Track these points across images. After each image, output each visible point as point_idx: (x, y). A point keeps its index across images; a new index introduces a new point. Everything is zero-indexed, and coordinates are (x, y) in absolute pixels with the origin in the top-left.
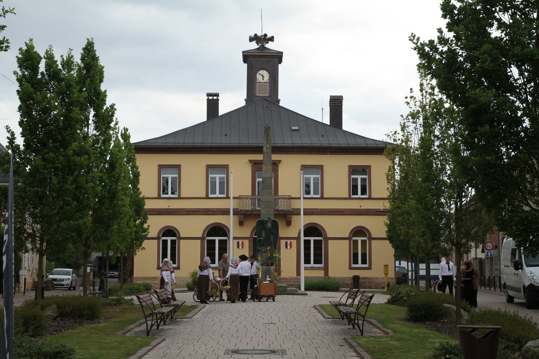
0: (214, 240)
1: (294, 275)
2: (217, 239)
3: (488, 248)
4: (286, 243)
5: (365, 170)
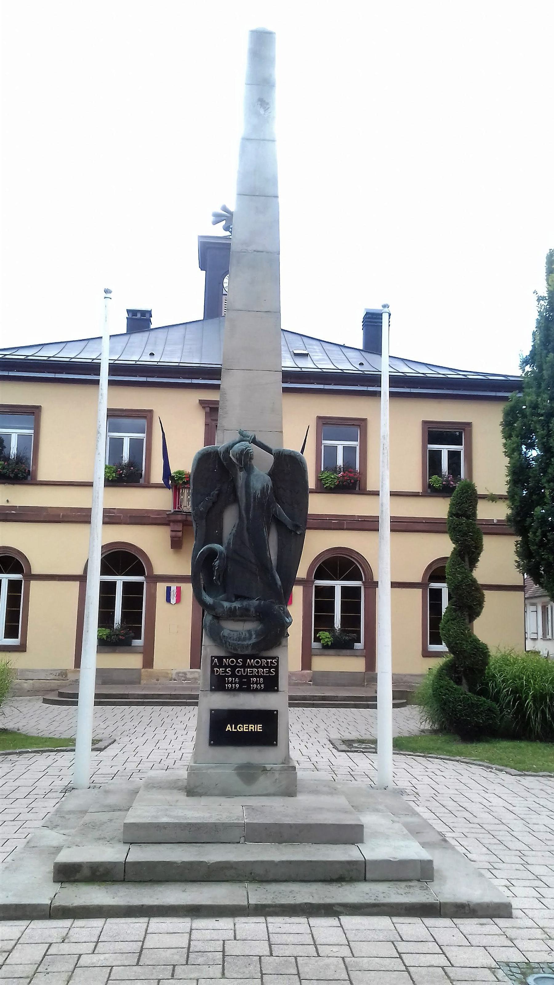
0: (333, 588)
1: (70, 665)
2: (338, 585)
4: (169, 589)
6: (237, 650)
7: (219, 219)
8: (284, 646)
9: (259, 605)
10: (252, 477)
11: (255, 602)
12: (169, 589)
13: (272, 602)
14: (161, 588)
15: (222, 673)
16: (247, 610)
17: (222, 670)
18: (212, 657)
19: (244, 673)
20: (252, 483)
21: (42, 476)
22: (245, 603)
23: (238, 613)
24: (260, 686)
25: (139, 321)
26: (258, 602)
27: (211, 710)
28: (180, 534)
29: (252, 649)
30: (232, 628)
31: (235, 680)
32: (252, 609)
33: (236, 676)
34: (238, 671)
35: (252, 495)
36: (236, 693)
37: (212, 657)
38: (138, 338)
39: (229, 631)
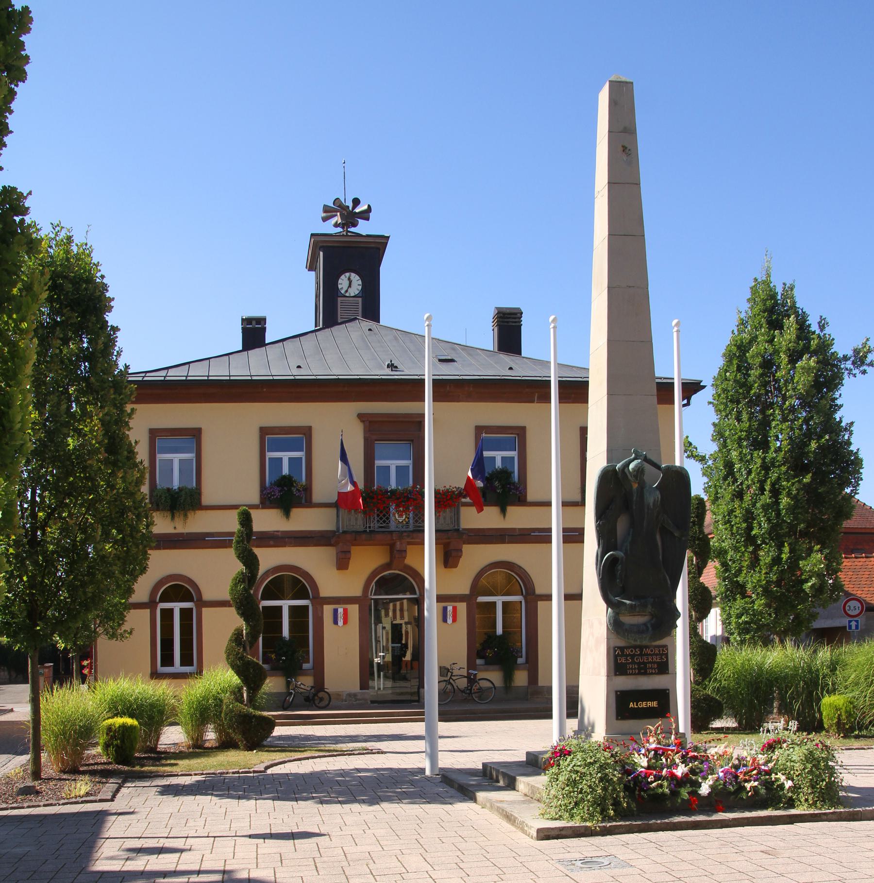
0: (280, 609)
3: (850, 613)
4: (336, 611)
5: (302, 437)
7: (365, 215)
14: (328, 610)
21: (530, 497)
25: (254, 333)
27: (616, 692)
38: (255, 354)
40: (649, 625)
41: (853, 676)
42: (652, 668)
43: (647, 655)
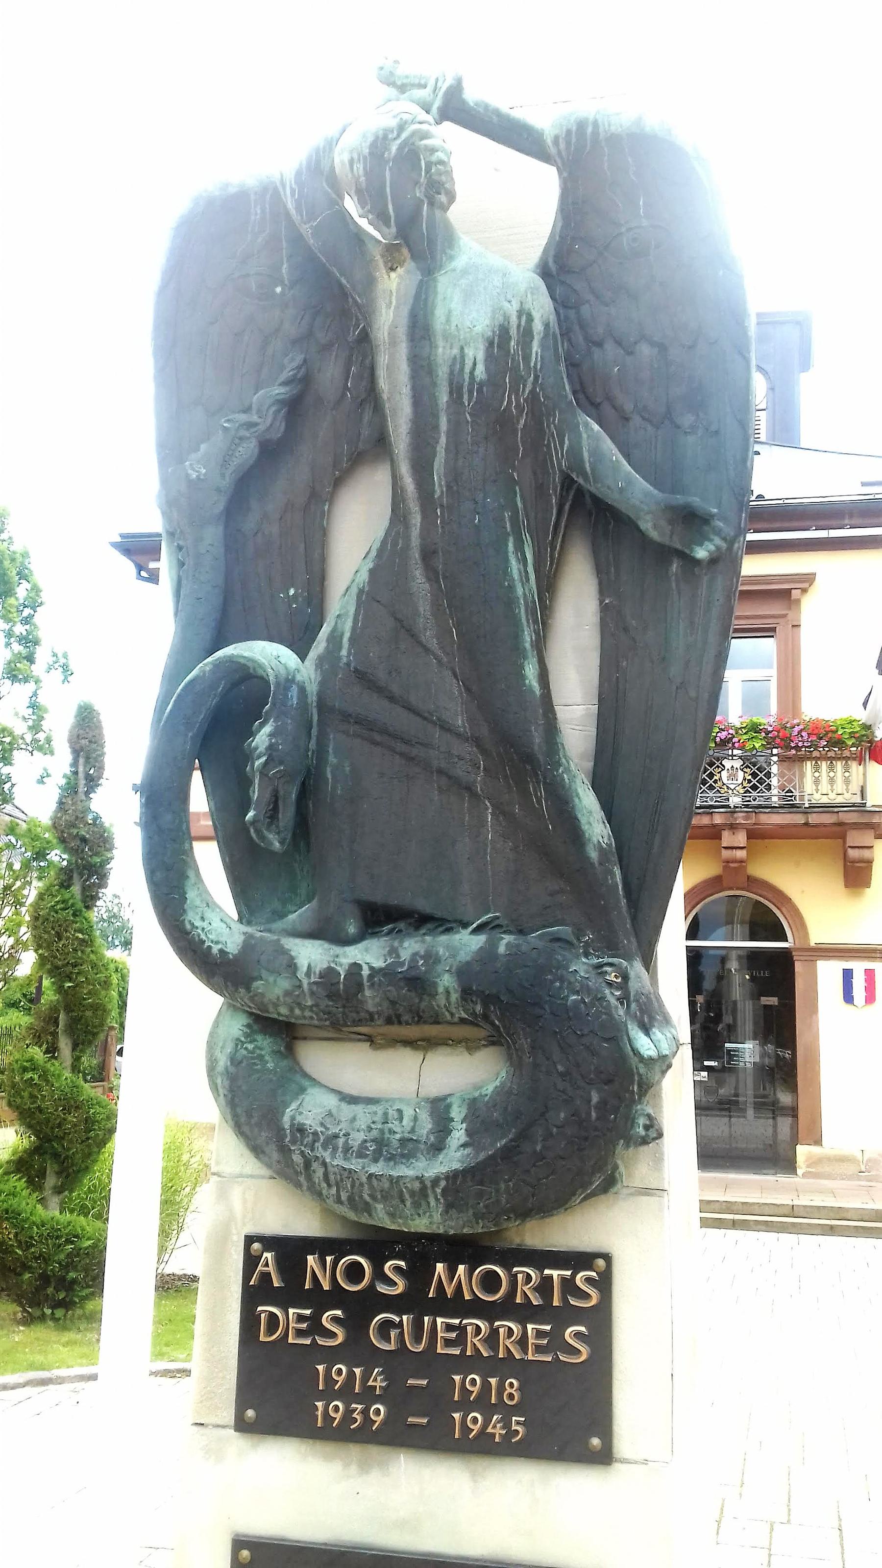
4: (848, 975)
6: (367, 1209)
8: (647, 1191)
9: (487, 955)
10: (443, 283)
11: (467, 943)
12: (848, 975)
13: (557, 940)
14: (828, 974)
15: (300, 1333)
16: (417, 982)
17: (300, 1318)
18: (250, 1240)
19: (418, 1339)
20: (440, 314)
22: (411, 947)
23: (370, 998)
24: (507, 1425)
26: (480, 940)
28: (741, 854)
29: (449, 1207)
30: (370, 1085)
31: (366, 1377)
32: (446, 981)
33: (369, 1357)
34: (386, 1326)
35: (442, 372)
36: (375, 1451)
37: (250, 1240)
39: (331, 1101)
40: (457, 1113)
41: (469, 439)
42: (483, 1403)
43: (457, 1305)
